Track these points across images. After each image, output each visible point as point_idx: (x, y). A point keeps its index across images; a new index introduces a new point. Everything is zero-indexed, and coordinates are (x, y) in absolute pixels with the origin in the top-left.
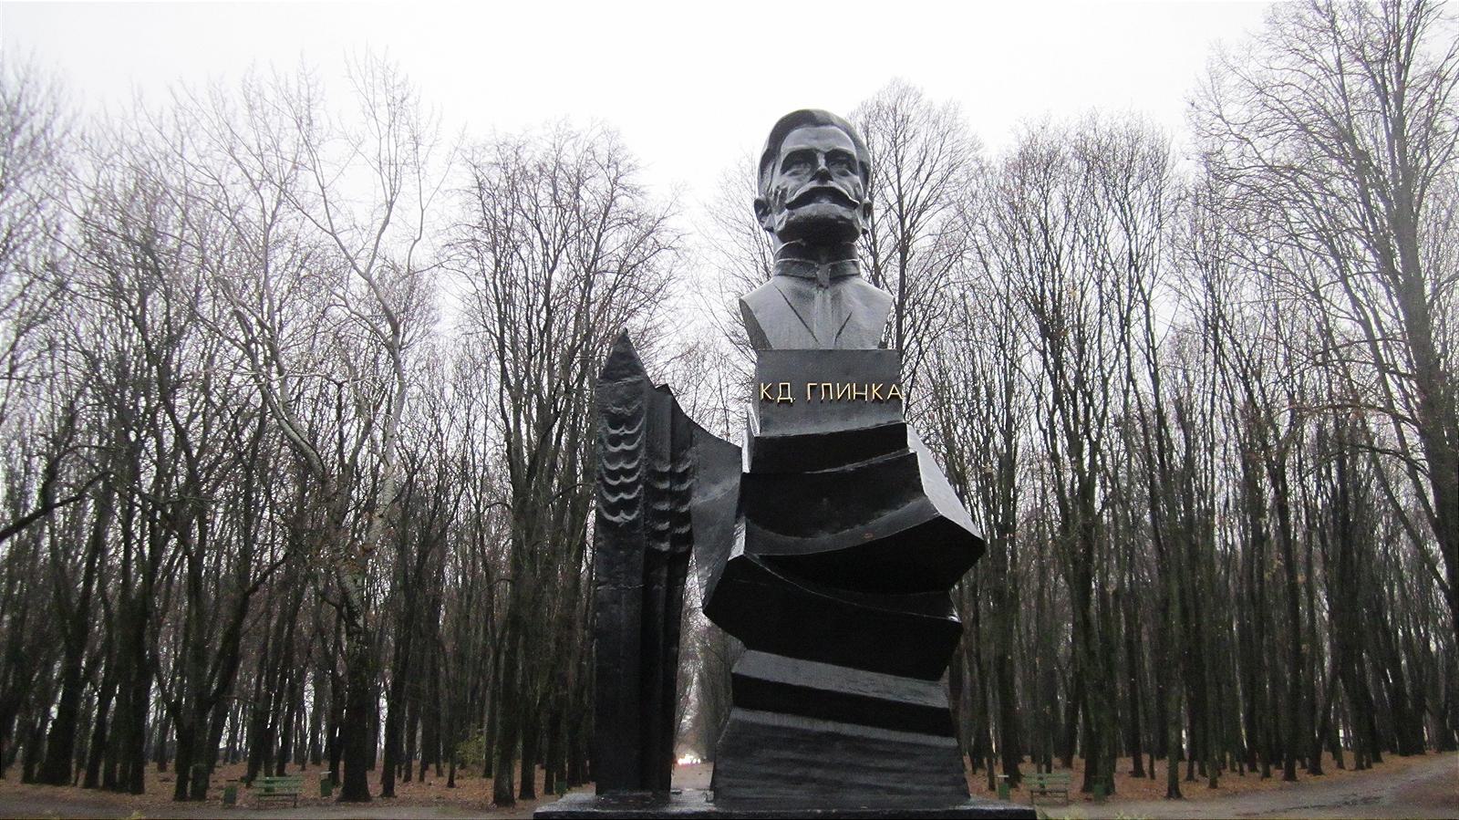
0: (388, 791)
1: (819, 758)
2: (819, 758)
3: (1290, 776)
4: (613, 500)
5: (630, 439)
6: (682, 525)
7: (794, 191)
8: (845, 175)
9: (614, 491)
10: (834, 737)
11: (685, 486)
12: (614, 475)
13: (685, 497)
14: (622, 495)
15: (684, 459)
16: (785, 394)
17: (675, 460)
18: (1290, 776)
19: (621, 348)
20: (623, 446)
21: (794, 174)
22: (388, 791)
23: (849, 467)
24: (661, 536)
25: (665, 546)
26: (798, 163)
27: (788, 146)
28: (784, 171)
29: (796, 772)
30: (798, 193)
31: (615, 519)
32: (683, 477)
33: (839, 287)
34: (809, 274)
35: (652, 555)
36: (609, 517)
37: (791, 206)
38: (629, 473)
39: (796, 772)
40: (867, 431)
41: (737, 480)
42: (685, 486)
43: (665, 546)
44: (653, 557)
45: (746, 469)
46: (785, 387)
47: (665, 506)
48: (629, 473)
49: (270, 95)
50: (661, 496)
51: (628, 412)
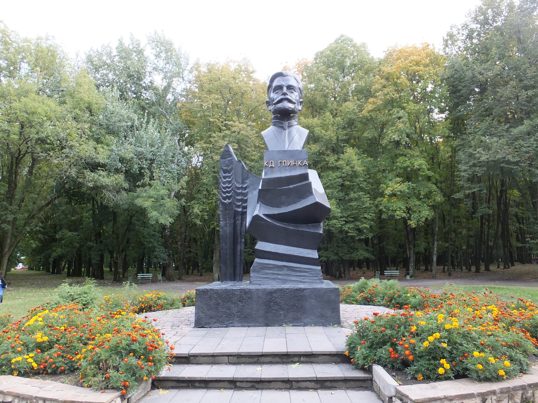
0: (192, 273)
1: (280, 273)
2: (280, 273)
3: (478, 270)
4: (224, 196)
5: (229, 177)
6: (244, 203)
7: (276, 99)
8: (292, 93)
9: (225, 193)
10: (285, 266)
11: (246, 191)
12: (225, 188)
13: (246, 195)
14: (227, 194)
15: (245, 183)
16: (272, 164)
17: (243, 183)
18: (478, 270)
19: (226, 149)
20: (227, 179)
21: (277, 93)
22: (192, 273)
23: (291, 186)
24: (238, 206)
25: (240, 210)
26: (278, 89)
27: (275, 84)
28: (273, 92)
29: (273, 277)
30: (277, 100)
31: (225, 202)
32: (245, 188)
33: (290, 129)
34: (281, 125)
35: (236, 212)
36: (223, 201)
37: (275, 104)
38: (229, 188)
39: (273, 277)
40: (294, 176)
41: (258, 190)
42: (246, 191)
43: (240, 210)
44: (236, 213)
45: (260, 188)
46: (272, 162)
47: (239, 198)
48: (229, 188)
49: (149, 53)
50: (239, 194)
51: (229, 169)
